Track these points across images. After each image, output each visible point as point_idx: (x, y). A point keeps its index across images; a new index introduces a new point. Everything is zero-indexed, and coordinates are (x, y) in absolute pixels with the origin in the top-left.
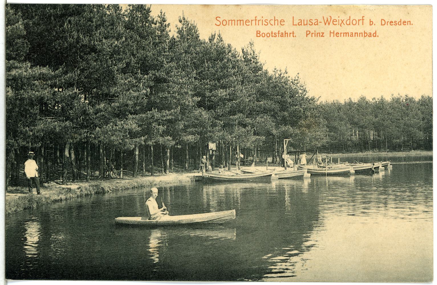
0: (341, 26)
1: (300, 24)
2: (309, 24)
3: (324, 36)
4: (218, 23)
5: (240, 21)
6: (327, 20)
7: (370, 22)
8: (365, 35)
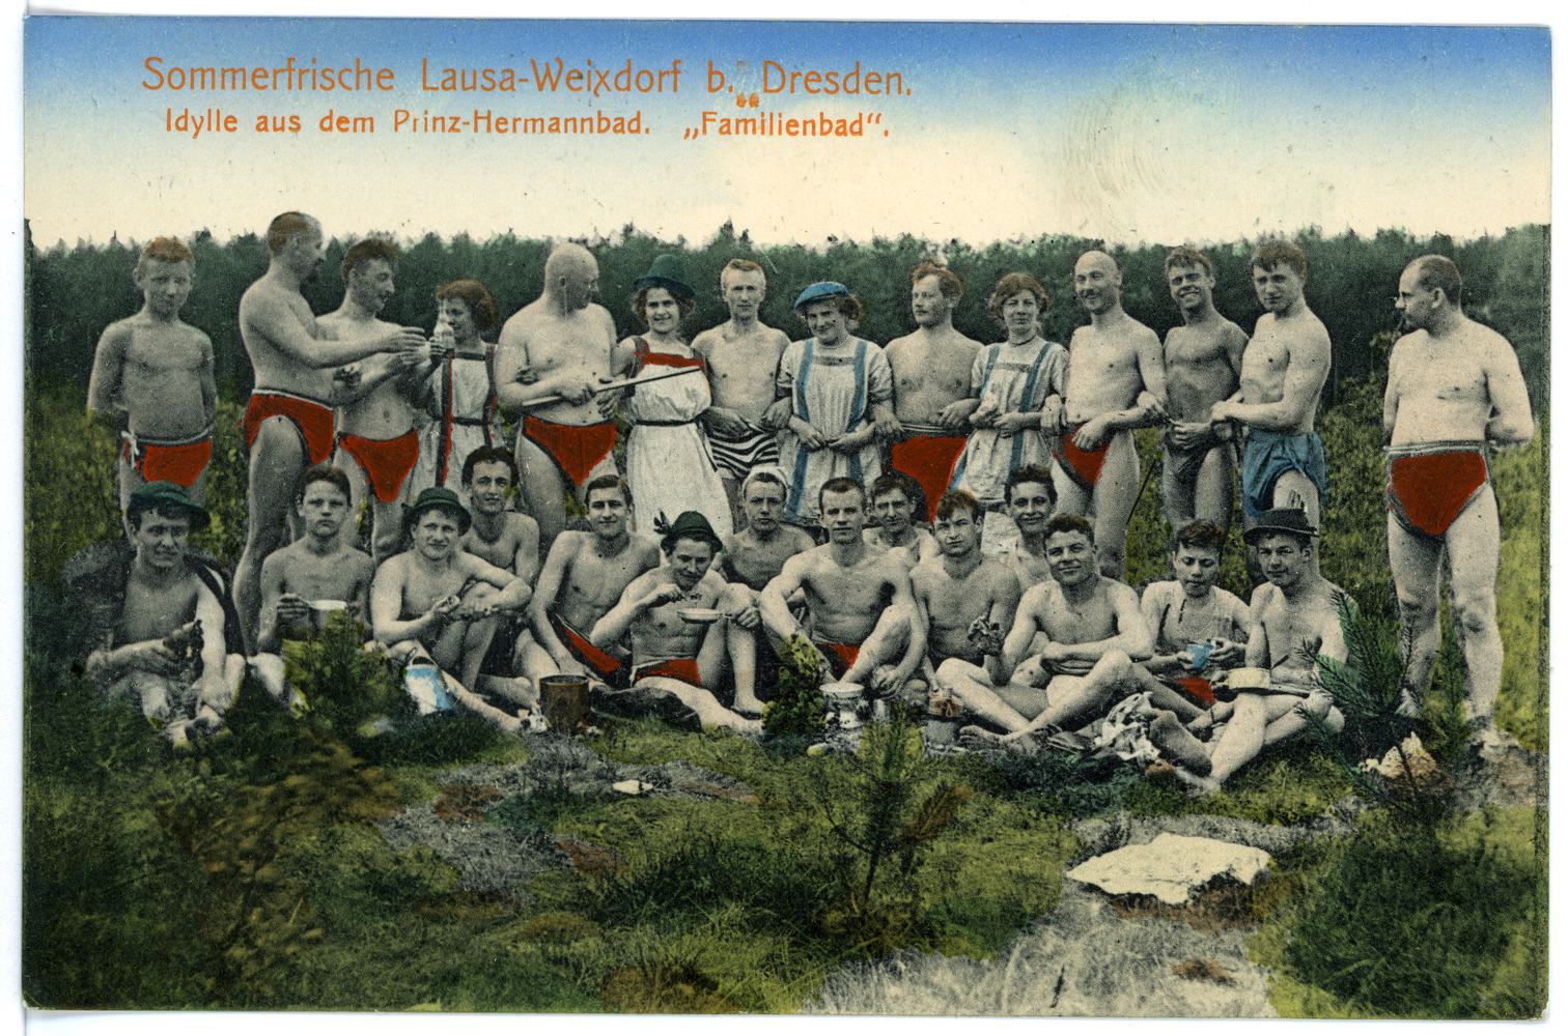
6: (548, 74)
8: (603, 128)
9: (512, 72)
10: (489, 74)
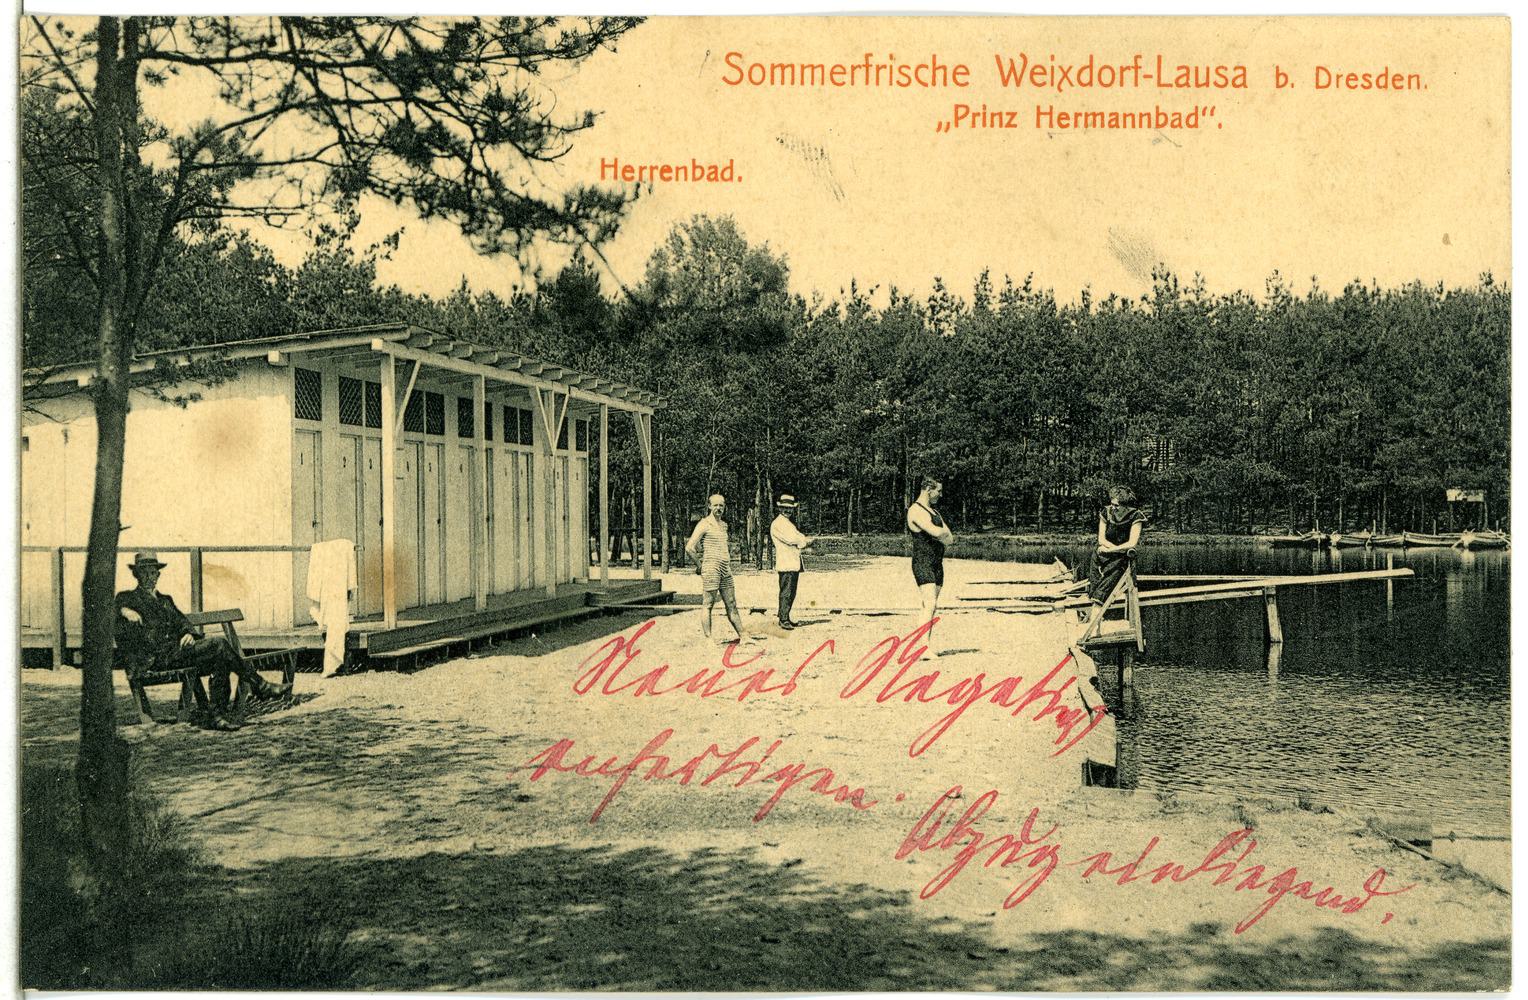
0: (1060, 90)
1: (1183, 81)
2: (898, 82)
3: (1015, 126)
4: (734, 76)
5: (813, 67)
6: (1013, 69)
7: (1278, 75)
9: (1244, 69)
10: (1221, 71)
